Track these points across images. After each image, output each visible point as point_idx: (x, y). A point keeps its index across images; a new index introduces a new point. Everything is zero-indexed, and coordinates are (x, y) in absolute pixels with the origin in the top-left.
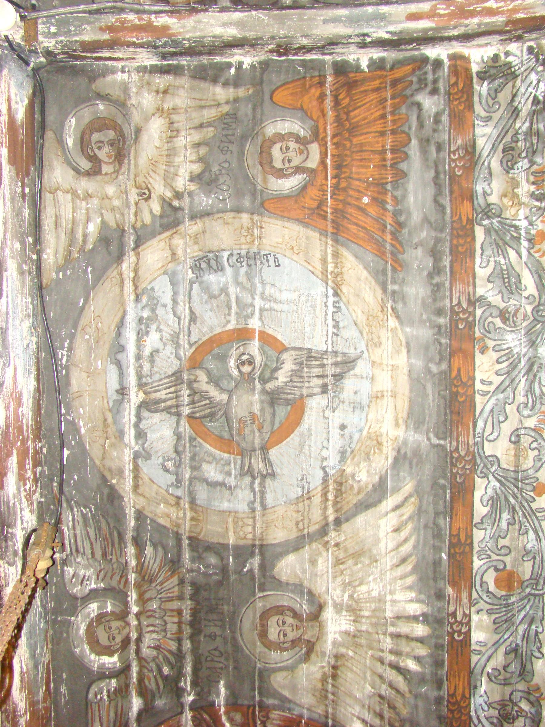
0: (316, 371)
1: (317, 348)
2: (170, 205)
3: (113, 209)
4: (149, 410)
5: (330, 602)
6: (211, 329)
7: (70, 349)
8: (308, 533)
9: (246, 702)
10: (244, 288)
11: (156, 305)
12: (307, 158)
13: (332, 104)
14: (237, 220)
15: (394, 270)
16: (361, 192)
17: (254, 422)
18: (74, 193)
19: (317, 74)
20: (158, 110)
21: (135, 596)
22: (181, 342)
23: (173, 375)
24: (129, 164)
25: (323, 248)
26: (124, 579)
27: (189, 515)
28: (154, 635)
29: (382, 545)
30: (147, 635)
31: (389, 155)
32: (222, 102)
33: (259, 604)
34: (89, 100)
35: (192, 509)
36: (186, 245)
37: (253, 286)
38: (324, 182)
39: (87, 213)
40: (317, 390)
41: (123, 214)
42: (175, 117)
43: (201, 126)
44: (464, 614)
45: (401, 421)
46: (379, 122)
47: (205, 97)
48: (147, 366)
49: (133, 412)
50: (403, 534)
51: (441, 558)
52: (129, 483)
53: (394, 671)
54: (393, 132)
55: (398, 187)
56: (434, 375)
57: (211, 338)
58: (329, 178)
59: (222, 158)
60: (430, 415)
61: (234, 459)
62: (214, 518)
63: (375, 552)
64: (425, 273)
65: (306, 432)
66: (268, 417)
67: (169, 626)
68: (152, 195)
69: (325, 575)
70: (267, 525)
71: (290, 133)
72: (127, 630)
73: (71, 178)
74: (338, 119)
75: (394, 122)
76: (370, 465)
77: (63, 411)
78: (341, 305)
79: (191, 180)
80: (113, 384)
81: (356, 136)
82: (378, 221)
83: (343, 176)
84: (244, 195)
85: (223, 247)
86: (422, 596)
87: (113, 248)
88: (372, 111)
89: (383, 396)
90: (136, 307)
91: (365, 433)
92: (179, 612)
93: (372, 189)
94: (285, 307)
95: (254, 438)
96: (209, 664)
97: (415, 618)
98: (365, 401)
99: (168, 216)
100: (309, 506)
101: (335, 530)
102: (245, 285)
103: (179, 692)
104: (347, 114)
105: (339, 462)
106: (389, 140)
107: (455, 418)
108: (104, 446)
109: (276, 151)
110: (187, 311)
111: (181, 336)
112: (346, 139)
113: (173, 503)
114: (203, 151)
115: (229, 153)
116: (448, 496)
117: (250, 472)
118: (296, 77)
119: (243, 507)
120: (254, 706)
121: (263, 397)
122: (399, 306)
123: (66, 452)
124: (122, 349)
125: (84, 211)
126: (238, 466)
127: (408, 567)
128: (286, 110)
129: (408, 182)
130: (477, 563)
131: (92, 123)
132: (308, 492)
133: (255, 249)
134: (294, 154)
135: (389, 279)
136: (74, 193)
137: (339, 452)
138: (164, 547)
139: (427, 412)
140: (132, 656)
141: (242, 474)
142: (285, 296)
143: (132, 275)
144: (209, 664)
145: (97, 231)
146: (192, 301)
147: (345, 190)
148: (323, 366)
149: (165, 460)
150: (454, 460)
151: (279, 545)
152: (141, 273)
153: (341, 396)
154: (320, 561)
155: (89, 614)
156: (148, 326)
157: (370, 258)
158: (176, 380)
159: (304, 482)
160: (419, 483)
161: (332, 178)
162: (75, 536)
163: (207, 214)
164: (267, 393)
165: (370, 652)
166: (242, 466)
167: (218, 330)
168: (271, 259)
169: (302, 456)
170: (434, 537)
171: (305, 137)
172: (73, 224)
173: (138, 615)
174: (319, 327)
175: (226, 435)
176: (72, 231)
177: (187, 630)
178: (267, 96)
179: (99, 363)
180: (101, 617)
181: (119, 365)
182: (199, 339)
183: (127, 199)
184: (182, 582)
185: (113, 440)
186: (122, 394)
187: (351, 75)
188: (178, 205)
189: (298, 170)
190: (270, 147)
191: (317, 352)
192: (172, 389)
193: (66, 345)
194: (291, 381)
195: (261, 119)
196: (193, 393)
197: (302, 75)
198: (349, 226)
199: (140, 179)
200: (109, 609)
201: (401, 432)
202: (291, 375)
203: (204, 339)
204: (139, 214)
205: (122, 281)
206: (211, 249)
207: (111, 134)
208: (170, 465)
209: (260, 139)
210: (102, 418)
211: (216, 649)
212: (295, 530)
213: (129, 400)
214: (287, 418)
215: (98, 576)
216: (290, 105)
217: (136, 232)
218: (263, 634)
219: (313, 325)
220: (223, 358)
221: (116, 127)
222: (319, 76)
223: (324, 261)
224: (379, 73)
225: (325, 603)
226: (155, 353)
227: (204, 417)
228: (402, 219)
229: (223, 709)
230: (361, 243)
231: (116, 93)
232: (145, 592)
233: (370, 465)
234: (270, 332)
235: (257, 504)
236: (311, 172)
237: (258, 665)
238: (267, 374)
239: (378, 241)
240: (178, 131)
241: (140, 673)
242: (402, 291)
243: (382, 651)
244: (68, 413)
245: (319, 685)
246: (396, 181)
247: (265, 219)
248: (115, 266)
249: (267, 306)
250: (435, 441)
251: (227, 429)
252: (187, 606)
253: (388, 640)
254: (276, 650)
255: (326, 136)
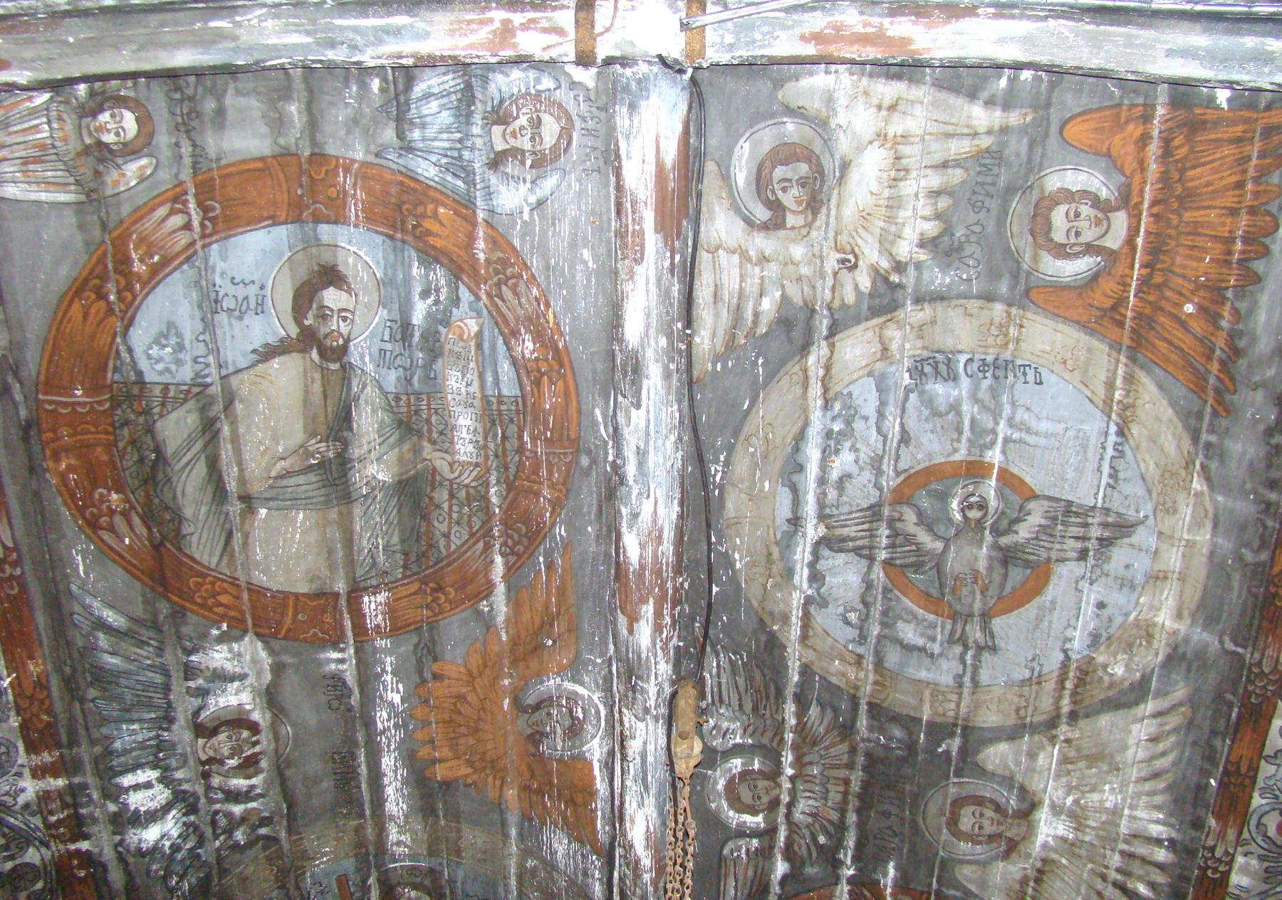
0: (1074, 531)
1: (1081, 502)
2: (886, 280)
3: (799, 279)
4: (831, 549)
5: (1047, 802)
6: (930, 456)
7: (727, 463)
8: (1031, 723)
9: (920, 888)
10: (984, 407)
11: (854, 416)
12: (1106, 232)
13: (1160, 152)
14: (984, 312)
15: (1215, 413)
16: (1185, 296)
17: (975, 582)
18: (744, 256)
19: (1140, 100)
20: (879, 135)
21: (790, 758)
22: (885, 467)
23: (869, 508)
24: (828, 215)
25: (1112, 368)
26: (778, 738)
27: (871, 677)
28: (811, 802)
29: (1130, 753)
30: (802, 801)
31: (1239, 246)
32: (982, 130)
33: (953, 790)
34: (773, 116)
35: (876, 671)
36: (904, 338)
37: (999, 406)
38: (1127, 271)
39: (762, 284)
40: (1074, 555)
41: (814, 288)
42: (905, 150)
43: (944, 165)
44: (1227, 853)
45: (1186, 613)
46: (1231, 193)
47: (953, 121)
48: (832, 494)
49: (808, 549)
50: (1161, 746)
51: (1208, 784)
52: (795, 631)
53: (1117, 891)
54: (1252, 211)
55: (1244, 296)
56: (1246, 565)
57: (927, 468)
58: (1137, 266)
59: (972, 218)
60: (1230, 614)
61: (943, 623)
62: (906, 686)
63: (1118, 758)
64: (1261, 427)
65: (1048, 604)
66: (997, 577)
67: (831, 795)
68: (860, 263)
69: (1046, 773)
70: (977, 706)
71: (1085, 191)
72: (777, 791)
73: (740, 234)
74: (1165, 178)
75: (1256, 194)
76: (1130, 659)
77: (713, 539)
78: (1126, 448)
79: (922, 244)
80: (784, 509)
81: (1190, 208)
82: (1201, 341)
83: (1159, 266)
84: (999, 277)
85: (960, 347)
86: (1173, 820)
87: (797, 334)
88: (1224, 174)
89: (1166, 578)
90: (824, 416)
91: (1131, 618)
92: (847, 782)
93: (1202, 293)
94: (1042, 441)
95: (974, 600)
96: (878, 842)
97: (1158, 842)
98: (1139, 578)
99: (880, 296)
100: (1037, 693)
101: (1068, 724)
102: (987, 403)
103: (837, 864)
104: (1182, 172)
105: (1089, 646)
106: (1243, 222)
107: (1265, 624)
108: (765, 586)
109: (1059, 217)
110: (897, 428)
111: (885, 461)
112: (1173, 212)
113: (852, 661)
114: (943, 203)
115: (984, 210)
116: (1234, 715)
117: (963, 641)
118: (1106, 104)
119: (946, 679)
120: (930, 894)
121: (994, 554)
122: (1214, 465)
123: (715, 589)
124: (800, 468)
125: (757, 281)
126: (947, 632)
127: (1161, 785)
128: (1083, 155)
129: (1262, 289)
130: (1257, 801)
131: (774, 152)
132: (1040, 676)
133: (1007, 355)
134: (1087, 224)
135: (1205, 426)
136: (744, 256)
137: (1090, 634)
138: (836, 710)
139: (1226, 608)
140: (781, 819)
141: (951, 641)
142: (1044, 426)
143: (821, 372)
144: (878, 842)
145: (775, 308)
146: (906, 415)
147: (1159, 287)
148: (1086, 525)
149: (846, 611)
150: (1253, 677)
151: (989, 729)
152: (834, 371)
153: (1105, 567)
154: (1041, 756)
155: (730, 770)
156: (838, 443)
157: (1180, 391)
158: (874, 515)
159: (1035, 664)
160: (1197, 690)
161: (1142, 266)
162: (720, 684)
163: (939, 298)
164: (1000, 548)
165: (1090, 866)
166: (953, 632)
167: (939, 459)
168: (1031, 373)
169: (1037, 634)
170: (1203, 758)
171: (1107, 201)
172: (740, 298)
173: (792, 779)
174: (1089, 475)
175: (935, 592)
176: (738, 307)
177: (853, 803)
178: (1054, 128)
179: (767, 484)
180: (745, 774)
181: (794, 489)
182: (912, 467)
183: (822, 266)
184: (853, 750)
185: (779, 579)
186: (795, 525)
187: (1198, 111)
188: (897, 281)
189: (1090, 249)
190: (1050, 209)
191: (1081, 506)
192: (866, 526)
193: (722, 458)
194: (1036, 538)
195: (1041, 164)
196: (895, 534)
197: (1117, 101)
198: (1157, 342)
199: (843, 239)
200: (756, 767)
201: (1183, 627)
202: (1038, 532)
203: (918, 468)
204: (838, 288)
205: (806, 378)
206: (942, 347)
207: (803, 168)
208: (853, 617)
209: (1035, 195)
210: (765, 551)
211: (889, 828)
212: (1013, 716)
213: (804, 535)
214: (1024, 583)
215: (745, 731)
216: (1090, 146)
217: (832, 314)
218: (953, 822)
219: (1080, 471)
220: (944, 497)
221: (810, 157)
222: (1145, 105)
223: (1110, 386)
224: (1245, 114)
225: (1041, 802)
226: (845, 478)
227: (907, 566)
228: (1241, 344)
229: (889, 890)
230: (1171, 369)
231: (815, 105)
232: (805, 754)
233: (1130, 659)
234: (1016, 471)
235: (967, 679)
236: (1111, 255)
237: (941, 853)
238: (1004, 524)
239: (1198, 371)
240: (907, 171)
241: (788, 838)
242: (1222, 444)
243: (1107, 867)
244: (720, 543)
245: (1017, 887)
246: (1242, 286)
247: (1029, 315)
248: (797, 358)
249: (1016, 436)
250: (1230, 646)
251: (937, 585)
252: (857, 777)
253: (1117, 857)
254: (966, 841)
255: (1141, 203)
